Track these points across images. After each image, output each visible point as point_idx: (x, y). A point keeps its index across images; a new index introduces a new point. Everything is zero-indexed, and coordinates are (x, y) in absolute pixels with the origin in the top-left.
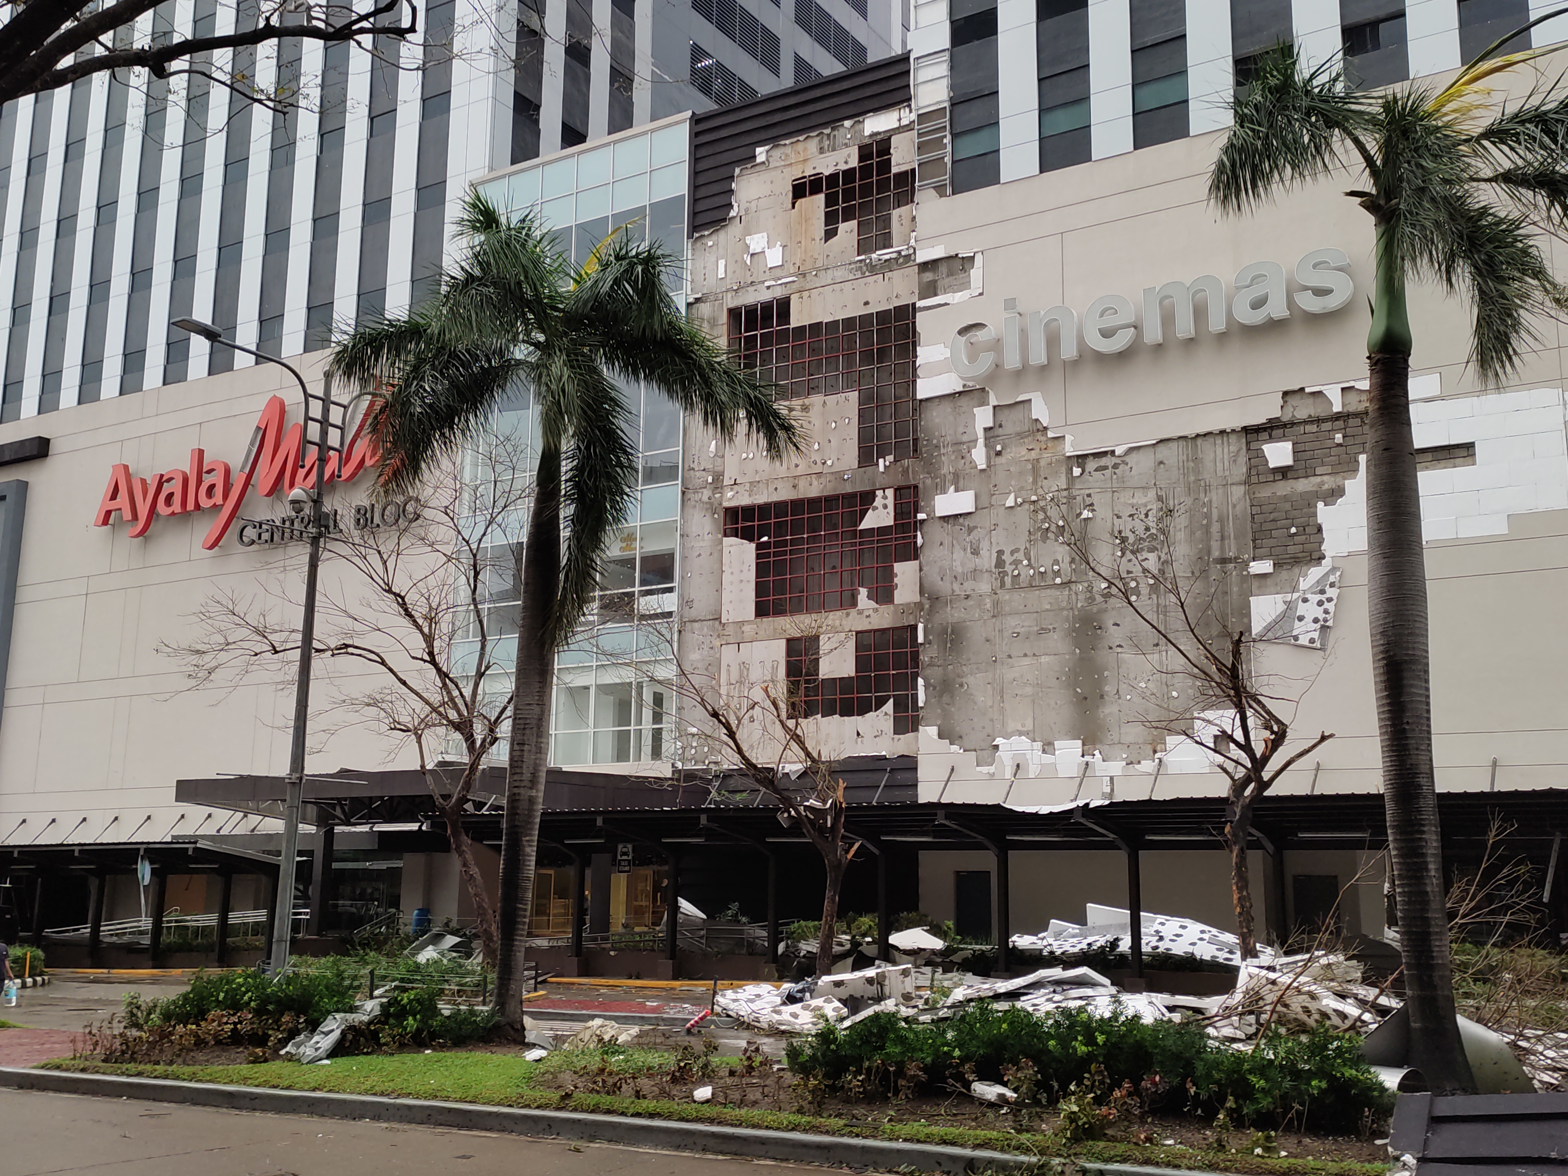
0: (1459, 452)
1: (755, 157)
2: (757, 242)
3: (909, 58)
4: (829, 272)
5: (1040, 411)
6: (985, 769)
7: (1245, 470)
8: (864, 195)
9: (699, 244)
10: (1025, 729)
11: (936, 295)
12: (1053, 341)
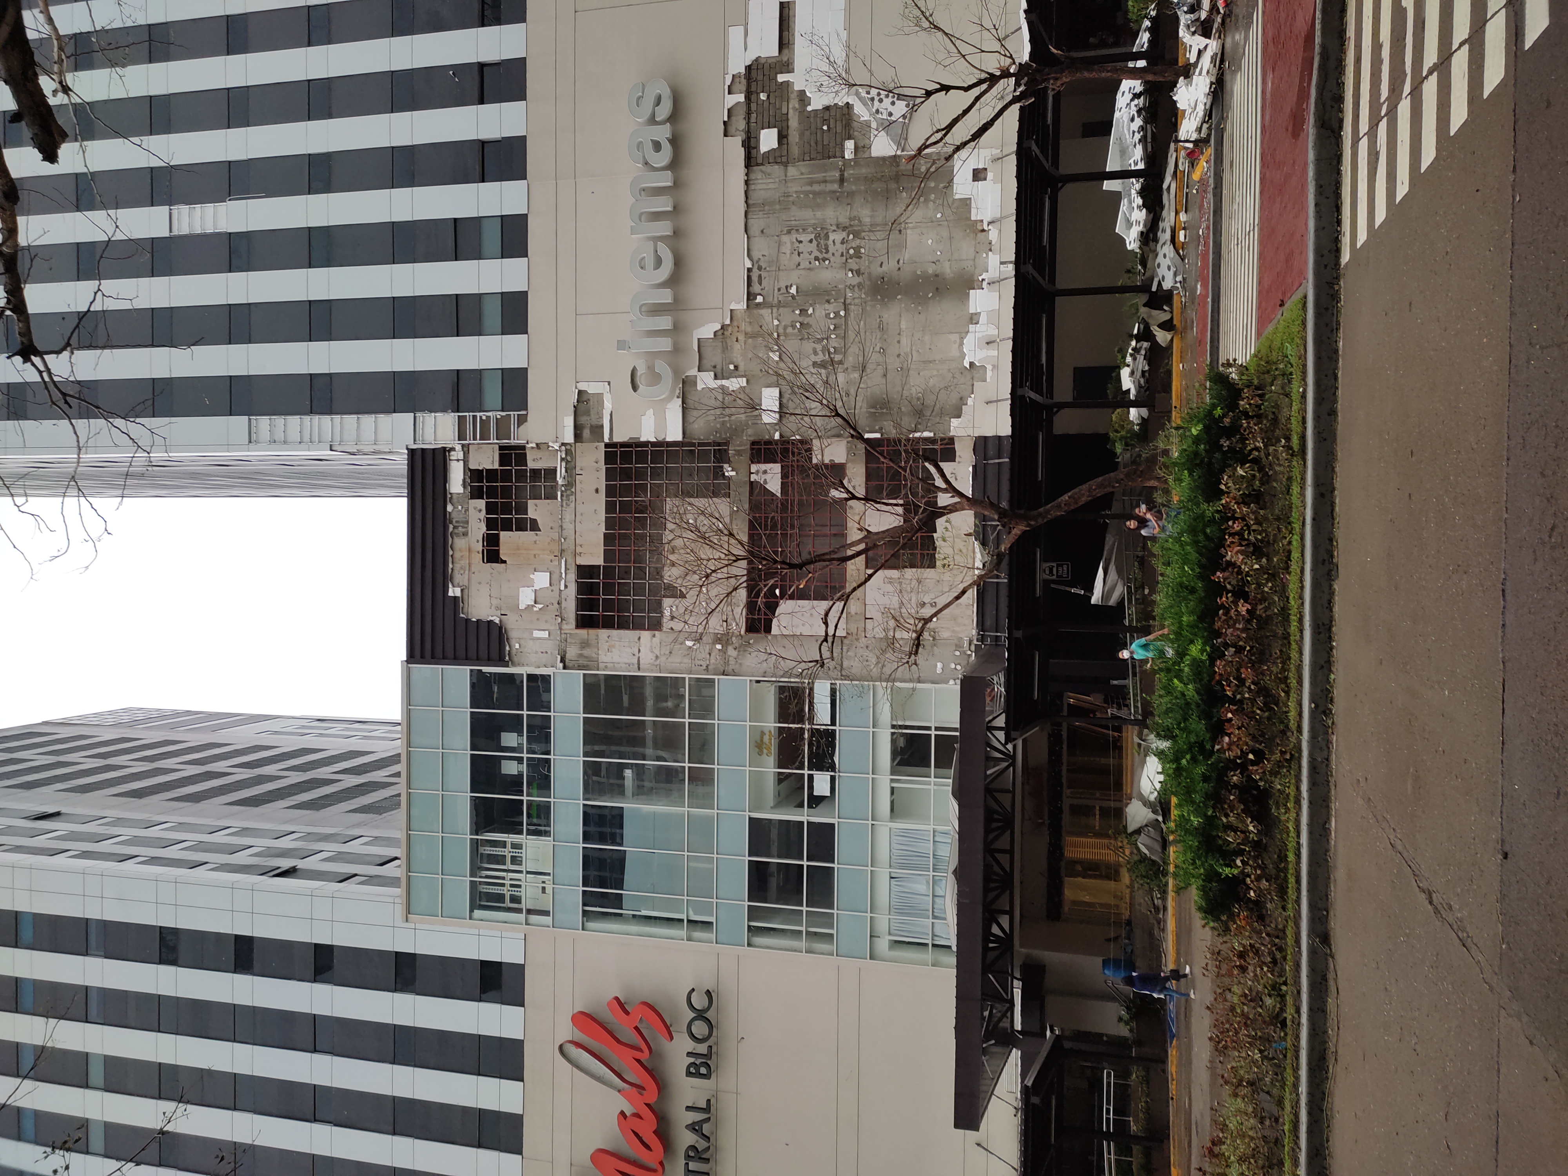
1: (455, 598)
2: (526, 597)
3: (412, 450)
4: (564, 526)
5: (707, 331)
6: (989, 373)
7: (777, 167)
8: (508, 490)
9: (515, 659)
10: (958, 341)
11: (602, 426)
12: (657, 310)
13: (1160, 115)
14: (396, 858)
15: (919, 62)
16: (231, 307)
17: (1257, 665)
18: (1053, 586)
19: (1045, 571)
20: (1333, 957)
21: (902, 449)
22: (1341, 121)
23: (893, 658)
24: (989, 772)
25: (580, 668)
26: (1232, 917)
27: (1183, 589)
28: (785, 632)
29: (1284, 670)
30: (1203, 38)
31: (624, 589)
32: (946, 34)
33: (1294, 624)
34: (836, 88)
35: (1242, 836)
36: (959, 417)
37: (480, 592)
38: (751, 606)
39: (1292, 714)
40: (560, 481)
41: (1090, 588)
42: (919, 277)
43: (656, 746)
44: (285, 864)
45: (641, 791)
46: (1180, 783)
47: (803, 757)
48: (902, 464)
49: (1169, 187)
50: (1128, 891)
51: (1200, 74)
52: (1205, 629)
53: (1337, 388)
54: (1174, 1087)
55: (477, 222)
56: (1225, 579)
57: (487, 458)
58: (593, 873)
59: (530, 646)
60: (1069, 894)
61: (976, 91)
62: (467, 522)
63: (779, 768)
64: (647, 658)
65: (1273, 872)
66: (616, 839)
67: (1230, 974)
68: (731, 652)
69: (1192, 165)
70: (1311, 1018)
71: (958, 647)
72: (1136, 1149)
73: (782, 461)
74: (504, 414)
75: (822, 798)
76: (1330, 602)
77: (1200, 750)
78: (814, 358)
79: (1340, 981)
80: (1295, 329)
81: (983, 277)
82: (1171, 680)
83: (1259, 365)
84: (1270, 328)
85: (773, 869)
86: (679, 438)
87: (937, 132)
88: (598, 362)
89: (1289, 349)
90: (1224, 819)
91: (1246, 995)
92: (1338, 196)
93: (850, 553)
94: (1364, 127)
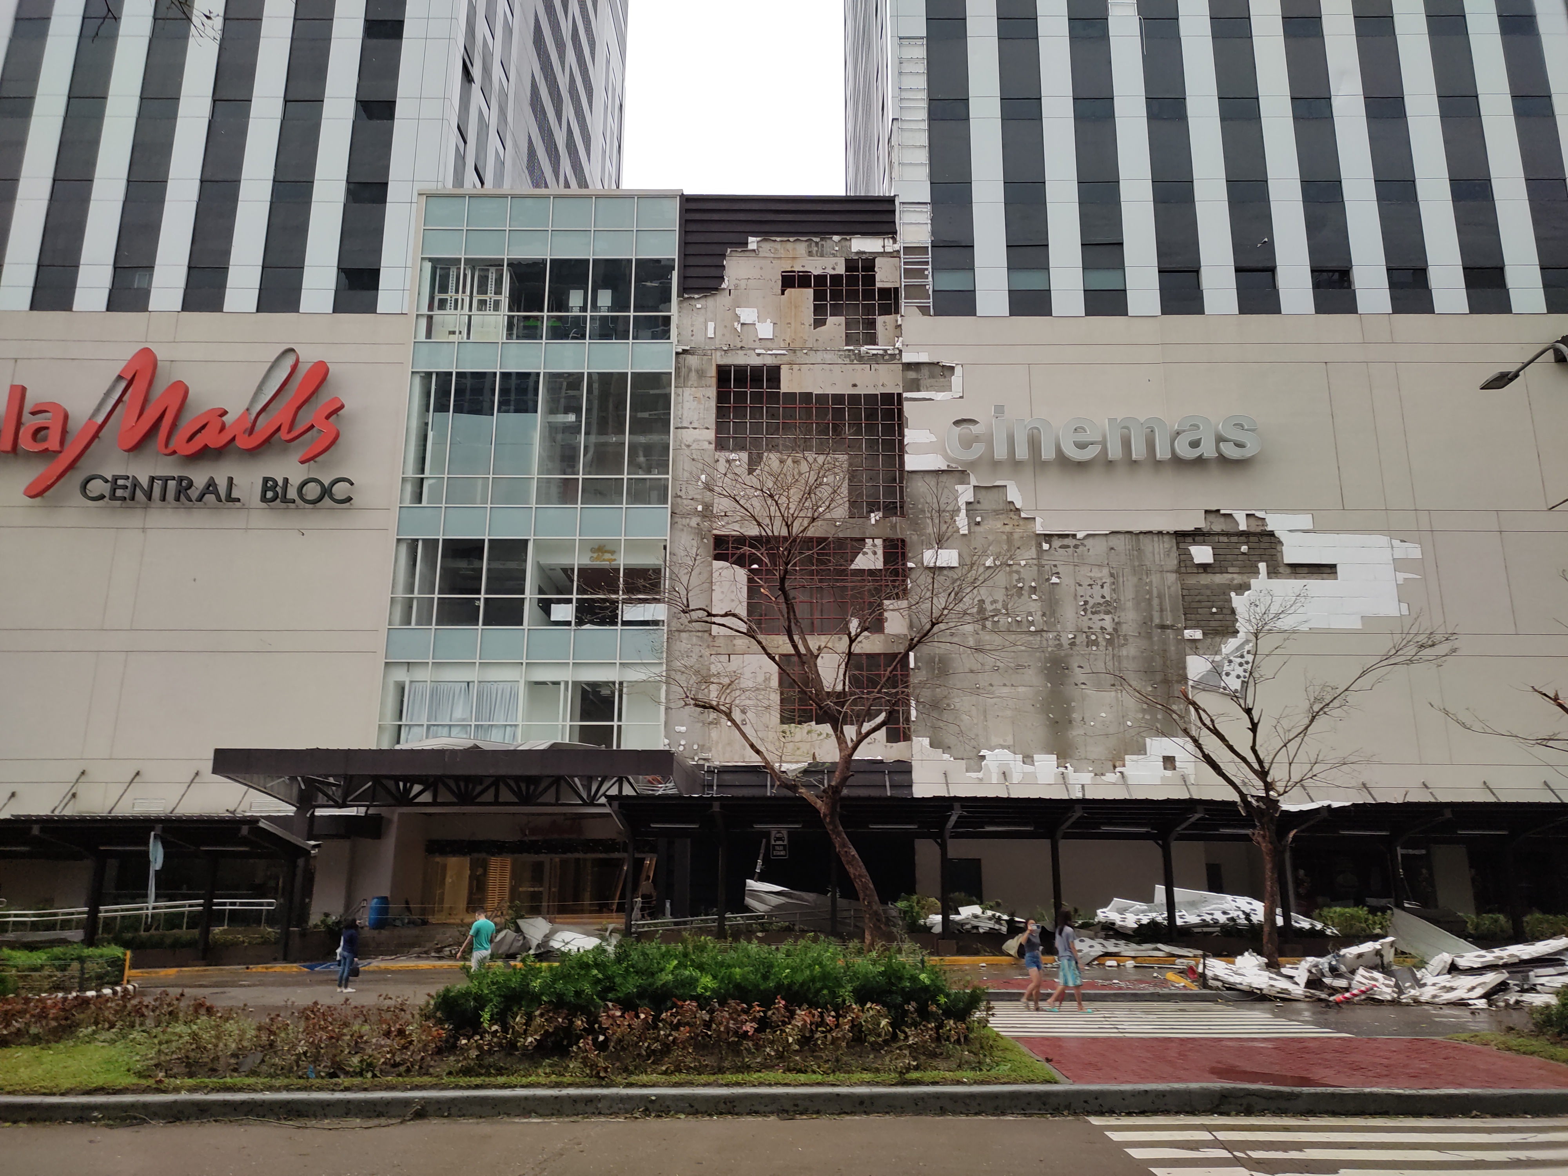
0: (1326, 570)
1: (747, 244)
2: (747, 315)
5: (1014, 495)
8: (855, 297)
9: (685, 304)
11: (919, 391)
12: (1034, 444)
13: (1229, 940)
14: (482, 183)
15: (1279, 702)
16: (1033, 19)
17: (692, 1041)
18: (764, 841)
19: (779, 833)
20: (401, 1123)
21: (899, 689)
22: (1228, 1114)
23: (691, 682)
24: (576, 780)
25: (678, 369)
26: (440, 1022)
27: (767, 969)
28: (715, 575)
29: (688, 1069)
30: (1305, 980)
31: (756, 412)
32: (1307, 728)
33: (733, 1078)
34: (1254, 621)
35: (522, 1031)
36: (931, 746)
37: (752, 268)
38: (741, 540)
39: (644, 1078)
40: (864, 349)
41: (762, 878)
42: (1069, 704)
43: (597, 445)
44: (476, 72)
45: (552, 430)
46: (573, 968)
47: (592, 594)
48: (884, 689)
49: (1160, 950)
50: (458, 921)
51: (1271, 978)
52: (727, 990)
53: (967, 1115)
54: (260, 970)
55: (1119, 265)
56: (777, 1009)
57: (886, 275)
58: (469, 382)
59: (699, 319)
60: (453, 861)
61: (1251, 758)
62: (822, 256)
63: (579, 569)
64: (688, 436)
65: (486, 1062)
66: (504, 407)
67: (381, 1021)
68: (694, 521)
69: (1181, 972)
70: (339, 1102)
71: (702, 747)
72: (196, 932)
73: (886, 570)
74: (931, 292)
75: (548, 612)
76: (756, 1112)
77: (607, 988)
78: (987, 602)
79: (378, 1129)
80: (1025, 1073)
81: (1069, 767)
82: (676, 957)
83: (988, 1038)
84: (1024, 1049)
85: (476, 564)
86: (908, 467)
87: (1212, 721)
88: (981, 385)
89: (1005, 1068)
90: (537, 1013)
91: (361, 1037)
92: (1155, 1112)
93: (796, 638)
94: (1222, 1136)
